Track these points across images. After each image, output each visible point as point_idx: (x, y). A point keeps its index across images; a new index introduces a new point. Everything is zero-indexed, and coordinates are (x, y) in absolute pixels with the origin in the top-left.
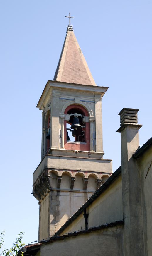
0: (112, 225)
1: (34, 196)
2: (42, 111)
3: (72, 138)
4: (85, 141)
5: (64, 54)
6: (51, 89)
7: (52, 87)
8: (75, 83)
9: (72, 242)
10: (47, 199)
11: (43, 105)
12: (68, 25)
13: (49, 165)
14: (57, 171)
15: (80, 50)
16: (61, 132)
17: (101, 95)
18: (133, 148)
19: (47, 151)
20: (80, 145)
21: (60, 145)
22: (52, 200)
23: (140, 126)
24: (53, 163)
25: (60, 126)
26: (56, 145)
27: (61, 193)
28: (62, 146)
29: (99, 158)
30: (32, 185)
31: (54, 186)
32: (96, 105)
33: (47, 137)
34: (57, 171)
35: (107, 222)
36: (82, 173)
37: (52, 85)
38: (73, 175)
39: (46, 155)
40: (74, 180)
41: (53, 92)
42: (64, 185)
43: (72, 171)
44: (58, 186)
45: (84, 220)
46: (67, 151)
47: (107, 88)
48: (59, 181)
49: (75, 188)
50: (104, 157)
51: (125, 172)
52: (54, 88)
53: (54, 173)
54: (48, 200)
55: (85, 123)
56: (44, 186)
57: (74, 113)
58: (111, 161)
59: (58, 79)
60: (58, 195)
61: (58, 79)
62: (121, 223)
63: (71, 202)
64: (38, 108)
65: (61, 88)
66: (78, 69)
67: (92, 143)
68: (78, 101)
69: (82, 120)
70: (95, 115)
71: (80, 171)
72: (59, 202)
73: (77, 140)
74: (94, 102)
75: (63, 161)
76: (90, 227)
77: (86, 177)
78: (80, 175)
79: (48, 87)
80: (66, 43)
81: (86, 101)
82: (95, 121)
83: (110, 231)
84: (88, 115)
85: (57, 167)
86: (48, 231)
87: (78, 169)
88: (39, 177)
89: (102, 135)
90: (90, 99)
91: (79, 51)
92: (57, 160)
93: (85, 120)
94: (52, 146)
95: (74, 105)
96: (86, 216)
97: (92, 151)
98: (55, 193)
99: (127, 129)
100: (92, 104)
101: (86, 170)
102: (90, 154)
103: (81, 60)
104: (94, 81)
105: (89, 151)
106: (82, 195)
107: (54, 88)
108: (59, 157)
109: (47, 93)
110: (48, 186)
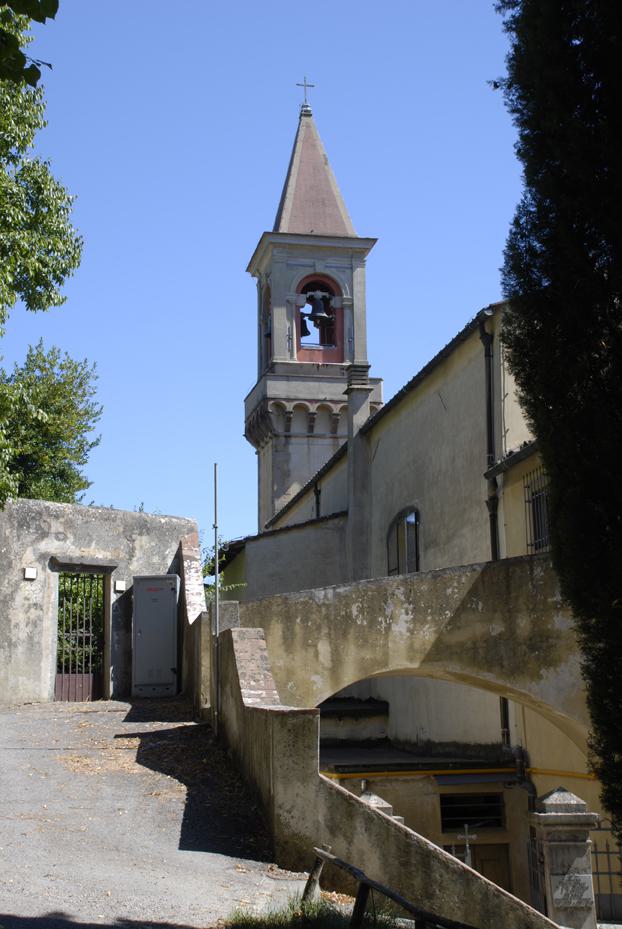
0: (335, 516)
1: (247, 439)
2: (256, 280)
3: (315, 334)
5: (294, 170)
6: (271, 247)
7: (272, 243)
8: (315, 233)
9: (284, 538)
10: (268, 450)
11: (258, 271)
12: (302, 102)
14: (284, 402)
15: (326, 159)
17: (363, 252)
19: (268, 367)
22: (276, 451)
24: (277, 389)
26: (281, 356)
27: (293, 440)
28: (292, 356)
30: (244, 419)
31: (279, 428)
32: (355, 273)
34: (284, 402)
36: (329, 404)
37: (272, 242)
38: (313, 408)
39: (265, 375)
40: (314, 417)
41: (275, 252)
42: (298, 426)
43: (311, 401)
44: (288, 429)
46: (301, 365)
47: (375, 240)
49: (317, 430)
51: (350, 449)
53: (279, 406)
54: (270, 452)
55: (335, 309)
56: (263, 427)
57: (314, 290)
58: (381, 380)
59: (284, 229)
60: (287, 443)
61: (284, 229)
62: (344, 514)
63: (309, 455)
64: (249, 274)
65: (289, 244)
66: (321, 198)
67: (347, 347)
68: (320, 269)
69: (329, 304)
70: (352, 295)
71: (325, 400)
72: (289, 455)
73: (323, 341)
74: (352, 268)
75: (294, 384)
77: (335, 412)
79: (265, 243)
80: (298, 144)
81: (336, 267)
82: (353, 305)
83: (331, 523)
84: (341, 295)
86: (274, 507)
87: (322, 397)
88: (255, 410)
89: (365, 331)
90: (345, 262)
91: (323, 160)
92: (285, 382)
93: (335, 303)
94: (275, 357)
96: (318, 493)
99: (354, 394)
100: (348, 271)
103: (327, 180)
104: (356, 229)
105: (342, 362)
106: (328, 441)
108: (287, 378)
109: (258, 260)
110: (270, 428)
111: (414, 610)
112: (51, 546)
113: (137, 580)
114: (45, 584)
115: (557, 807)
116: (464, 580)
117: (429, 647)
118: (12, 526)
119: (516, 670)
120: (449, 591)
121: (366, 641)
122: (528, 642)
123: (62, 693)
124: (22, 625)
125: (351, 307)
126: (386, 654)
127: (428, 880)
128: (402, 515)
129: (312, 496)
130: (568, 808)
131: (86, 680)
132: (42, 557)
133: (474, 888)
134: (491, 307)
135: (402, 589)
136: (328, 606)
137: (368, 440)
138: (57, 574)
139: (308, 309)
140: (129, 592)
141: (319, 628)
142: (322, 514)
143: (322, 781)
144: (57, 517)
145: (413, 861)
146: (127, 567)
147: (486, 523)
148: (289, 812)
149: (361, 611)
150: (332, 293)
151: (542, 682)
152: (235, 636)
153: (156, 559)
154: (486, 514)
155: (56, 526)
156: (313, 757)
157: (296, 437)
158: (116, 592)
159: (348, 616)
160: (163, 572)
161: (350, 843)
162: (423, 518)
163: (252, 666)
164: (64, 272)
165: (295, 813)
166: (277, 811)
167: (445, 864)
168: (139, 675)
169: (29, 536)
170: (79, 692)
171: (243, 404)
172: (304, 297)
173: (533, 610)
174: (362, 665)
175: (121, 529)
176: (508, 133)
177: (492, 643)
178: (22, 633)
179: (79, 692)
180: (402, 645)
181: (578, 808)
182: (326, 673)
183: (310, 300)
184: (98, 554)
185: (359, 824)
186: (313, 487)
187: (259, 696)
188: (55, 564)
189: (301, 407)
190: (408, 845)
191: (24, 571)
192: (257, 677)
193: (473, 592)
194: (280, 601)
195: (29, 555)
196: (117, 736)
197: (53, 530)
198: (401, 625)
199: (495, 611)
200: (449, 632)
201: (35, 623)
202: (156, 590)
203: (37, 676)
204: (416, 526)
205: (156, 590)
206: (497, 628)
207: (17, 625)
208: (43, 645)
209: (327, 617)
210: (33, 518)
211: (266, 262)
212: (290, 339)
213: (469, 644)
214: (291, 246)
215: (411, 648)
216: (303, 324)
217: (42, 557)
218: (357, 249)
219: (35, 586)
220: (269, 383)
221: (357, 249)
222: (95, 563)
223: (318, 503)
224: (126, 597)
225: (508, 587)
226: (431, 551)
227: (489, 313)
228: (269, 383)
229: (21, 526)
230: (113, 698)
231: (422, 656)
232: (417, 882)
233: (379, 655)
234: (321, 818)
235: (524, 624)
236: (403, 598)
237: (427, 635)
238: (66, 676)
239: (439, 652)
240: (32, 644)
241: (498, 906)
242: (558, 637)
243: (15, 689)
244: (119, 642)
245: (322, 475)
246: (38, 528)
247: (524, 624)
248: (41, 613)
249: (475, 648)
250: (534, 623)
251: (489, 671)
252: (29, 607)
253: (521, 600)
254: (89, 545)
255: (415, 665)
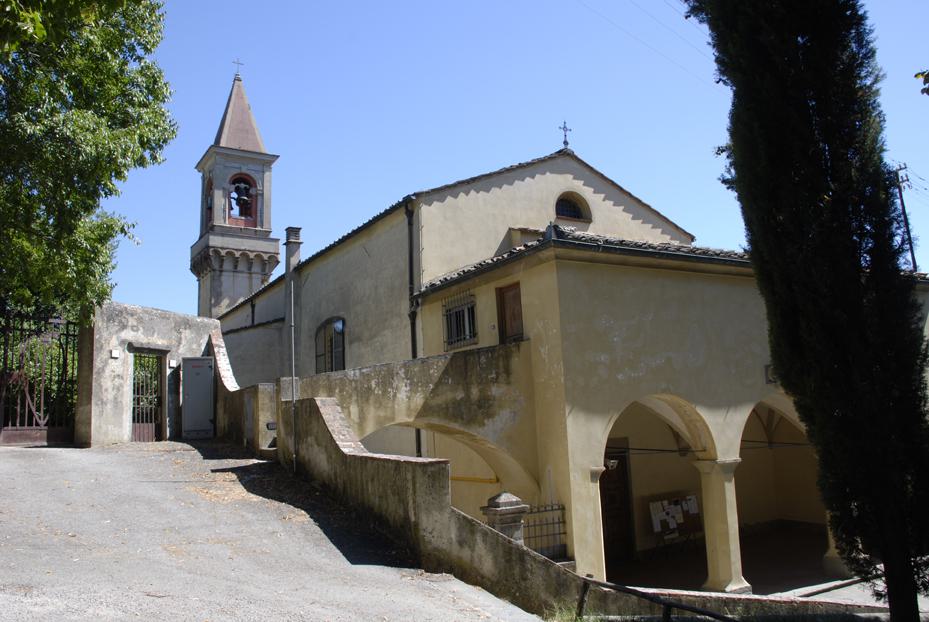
0: (276, 321)
2: (201, 174)
3: (236, 210)
4: (250, 215)
5: (230, 110)
10: (207, 279)
13: (211, 244)
16: (225, 206)
18: (294, 262)
19: (207, 226)
20: (245, 221)
21: (222, 221)
23: (301, 243)
24: (215, 241)
25: (223, 201)
27: (224, 273)
29: (265, 236)
33: (208, 210)
35: (271, 319)
38: (237, 254)
42: (227, 265)
43: (236, 250)
44: (221, 266)
45: (250, 310)
47: (278, 157)
48: (223, 260)
50: (272, 236)
52: (218, 154)
53: (216, 252)
60: (220, 275)
66: (246, 128)
67: (259, 219)
68: (244, 170)
73: (241, 214)
76: (256, 323)
78: (244, 254)
84: (256, 187)
85: (220, 245)
87: (243, 248)
88: (199, 253)
90: (259, 168)
93: (252, 191)
95: (241, 174)
96: (253, 306)
97: (259, 228)
98: (218, 273)
101: (252, 249)
102: (256, 231)
104: (267, 148)
107: (218, 154)
108: (223, 235)
110: (210, 265)
111: (410, 384)
112: (128, 335)
113: (184, 360)
114: (125, 362)
115: (506, 504)
116: (440, 364)
117: (419, 408)
118: (103, 320)
119: (471, 421)
120: (432, 371)
121: (381, 404)
122: (491, 402)
123: (137, 436)
124: (110, 390)
125: (262, 195)
126: (394, 413)
127: (524, 569)
128: (339, 319)
129: (248, 308)
130: (511, 504)
131: (150, 427)
132: (122, 342)
133: (552, 571)
134: (415, 194)
135: (403, 370)
136: (356, 381)
137: (299, 274)
138: (132, 354)
139: (234, 195)
140: (179, 367)
141: (351, 396)
142: (256, 323)
143: (453, 511)
144: (132, 315)
145: (514, 558)
146: (176, 351)
147: (405, 327)
148: (431, 533)
149: (377, 384)
150: (251, 186)
151: (486, 428)
152: (318, 403)
153: (194, 346)
154: (407, 322)
155: (132, 321)
156: (446, 494)
157: (226, 271)
158: (170, 368)
159: (369, 388)
160: (199, 355)
161: (473, 551)
162: (348, 323)
163: (337, 425)
164: (165, 141)
165: (435, 533)
166: (422, 533)
167: (534, 558)
168: (187, 425)
169: (114, 327)
170: (146, 436)
171: (189, 251)
172: (233, 187)
173: (480, 384)
174: (380, 421)
175: (173, 325)
176: (710, 53)
177: (457, 404)
178: (109, 395)
179: (146, 436)
180: (403, 406)
181: (517, 503)
182: (356, 426)
183: (237, 190)
184: (158, 342)
185: (479, 538)
186: (251, 301)
187: (350, 446)
188: (131, 347)
189: (258, 256)
190: (511, 548)
191: (111, 352)
192: (343, 432)
193: (446, 372)
194: (325, 378)
195: (114, 341)
196: (213, 471)
197: (130, 324)
198: (403, 394)
199: (458, 384)
200: (433, 398)
201: (118, 389)
202: (199, 367)
203: (120, 425)
204: (342, 333)
205: (199, 367)
206: (460, 395)
207: (106, 390)
208: (124, 403)
209: (356, 388)
210: (117, 315)
211: (209, 163)
212: (224, 211)
213: (444, 406)
214: (228, 155)
215: (409, 408)
216: (230, 203)
217: (122, 342)
218: (267, 161)
219: (118, 362)
220: (211, 237)
221: (267, 161)
222: (157, 348)
223: (253, 312)
224: (176, 371)
225: (466, 369)
226: (356, 344)
227: (414, 198)
228: (211, 237)
229: (109, 320)
230: (171, 439)
231: (416, 414)
232: (517, 571)
233: (389, 414)
234: (453, 536)
235: (475, 392)
236: (403, 376)
237: (419, 400)
238: (142, 425)
239: (426, 410)
240: (116, 402)
241: (566, 580)
242: (494, 400)
243: (106, 434)
244: (172, 402)
245: (257, 295)
246: (120, 322)
247: (475, 392)
248: (122, 381)
249: (447, 408)
250: (480, 391)
251: (455, 422)
252: (114, 377)
253: (473, 378)
254: (153, 335)
255: (411, 420)
